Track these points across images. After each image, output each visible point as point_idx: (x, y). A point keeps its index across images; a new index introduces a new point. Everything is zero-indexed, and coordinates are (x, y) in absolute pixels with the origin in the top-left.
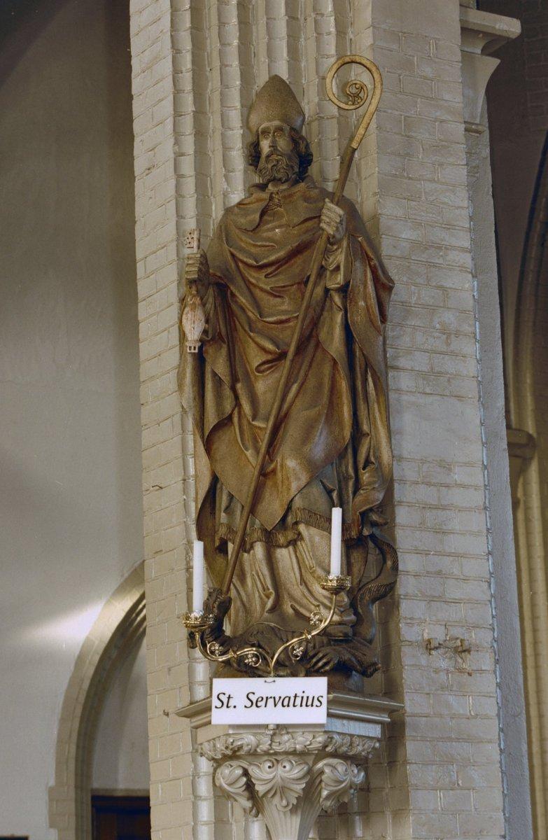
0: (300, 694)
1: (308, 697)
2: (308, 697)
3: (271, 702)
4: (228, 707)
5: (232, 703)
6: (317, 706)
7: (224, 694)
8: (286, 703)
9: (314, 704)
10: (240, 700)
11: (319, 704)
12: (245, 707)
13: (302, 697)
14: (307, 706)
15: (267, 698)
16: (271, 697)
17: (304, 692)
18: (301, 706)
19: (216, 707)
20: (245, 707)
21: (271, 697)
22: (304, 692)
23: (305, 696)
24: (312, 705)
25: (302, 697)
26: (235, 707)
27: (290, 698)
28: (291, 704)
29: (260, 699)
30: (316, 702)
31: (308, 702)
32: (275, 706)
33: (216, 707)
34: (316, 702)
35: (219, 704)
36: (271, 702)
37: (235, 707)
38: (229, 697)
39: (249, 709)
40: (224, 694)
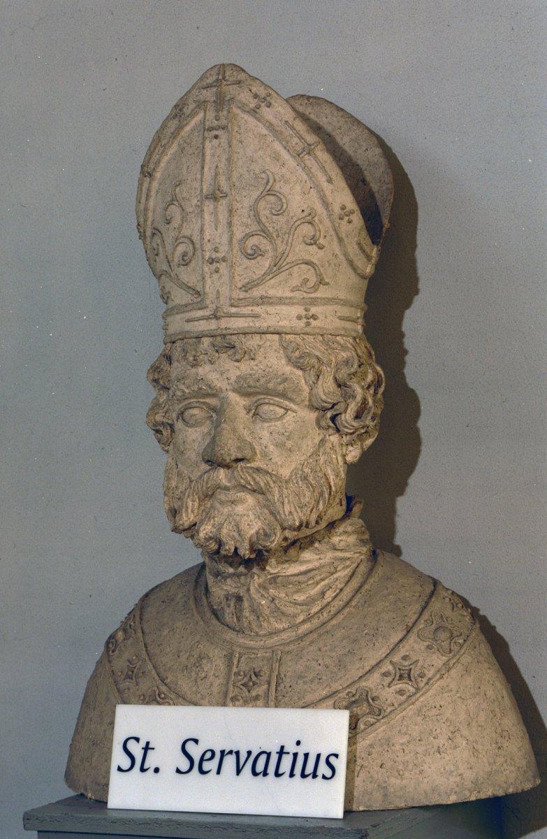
0: (291, 748)
1: (306, 755)
2: (306, 755)
3: (230, 762)
4: (143, 770)
5: (151, 762)
6: (324, 777)
7: (137, 740)
8: (260, 767)
9: (320, 773)
10: (167, 756)
11: (328, 773)
12: (178, 771)
13: (295, 755)
14: (277, 774)
15: (222, 752)
16: (231, 752)
17: (298, 743)
18: (292, 775)
19: (120, 769)
20: (178, 771)
21: (231, 752)
22: (298, 743)
23: (301, 751)
24: (315, 776)
25: (295, 755)
26: (157, 770)
27: (269, 755)
28: (271, 769)
29: (208, 755)
30: (323, 769)
31: (309, 767)
32: (239, 771)
33: (120, 769)
34: (323, 769)
35: (126, 763)
36: (230, 762)
37: (157, 770)
38: (147, 748)
39: (326, 781)
40: (137, 740)
